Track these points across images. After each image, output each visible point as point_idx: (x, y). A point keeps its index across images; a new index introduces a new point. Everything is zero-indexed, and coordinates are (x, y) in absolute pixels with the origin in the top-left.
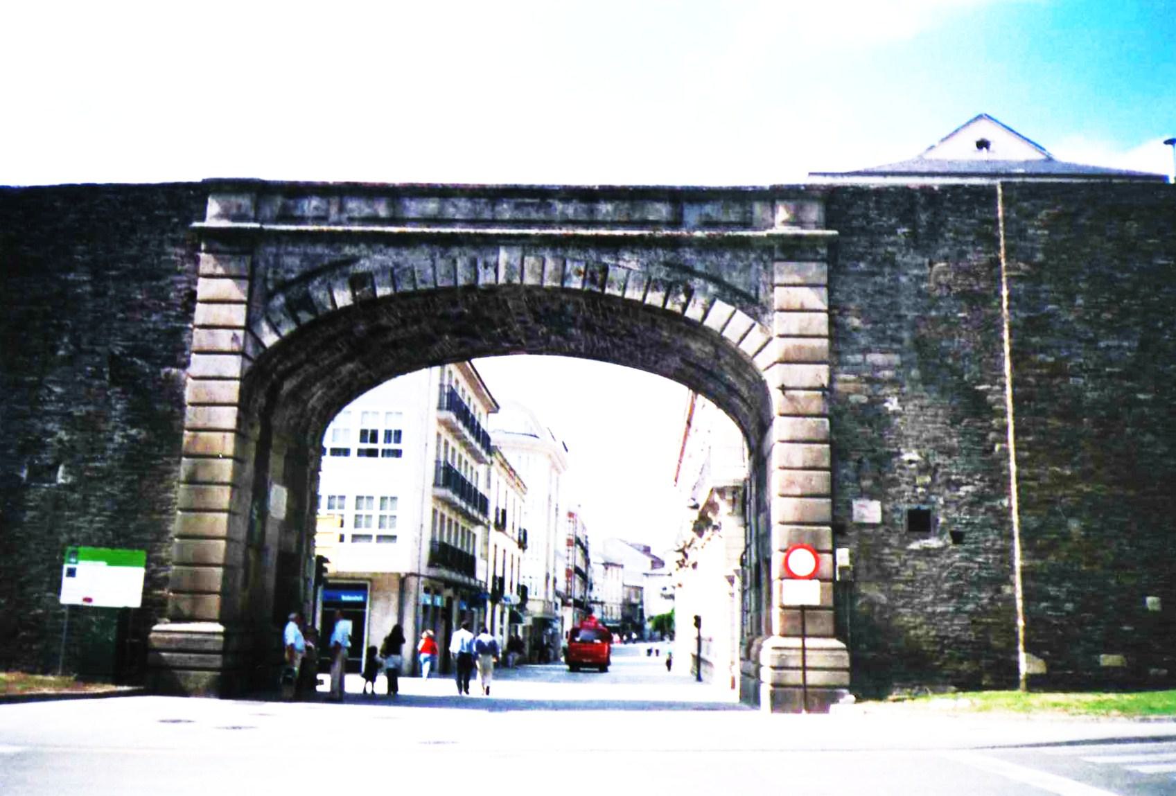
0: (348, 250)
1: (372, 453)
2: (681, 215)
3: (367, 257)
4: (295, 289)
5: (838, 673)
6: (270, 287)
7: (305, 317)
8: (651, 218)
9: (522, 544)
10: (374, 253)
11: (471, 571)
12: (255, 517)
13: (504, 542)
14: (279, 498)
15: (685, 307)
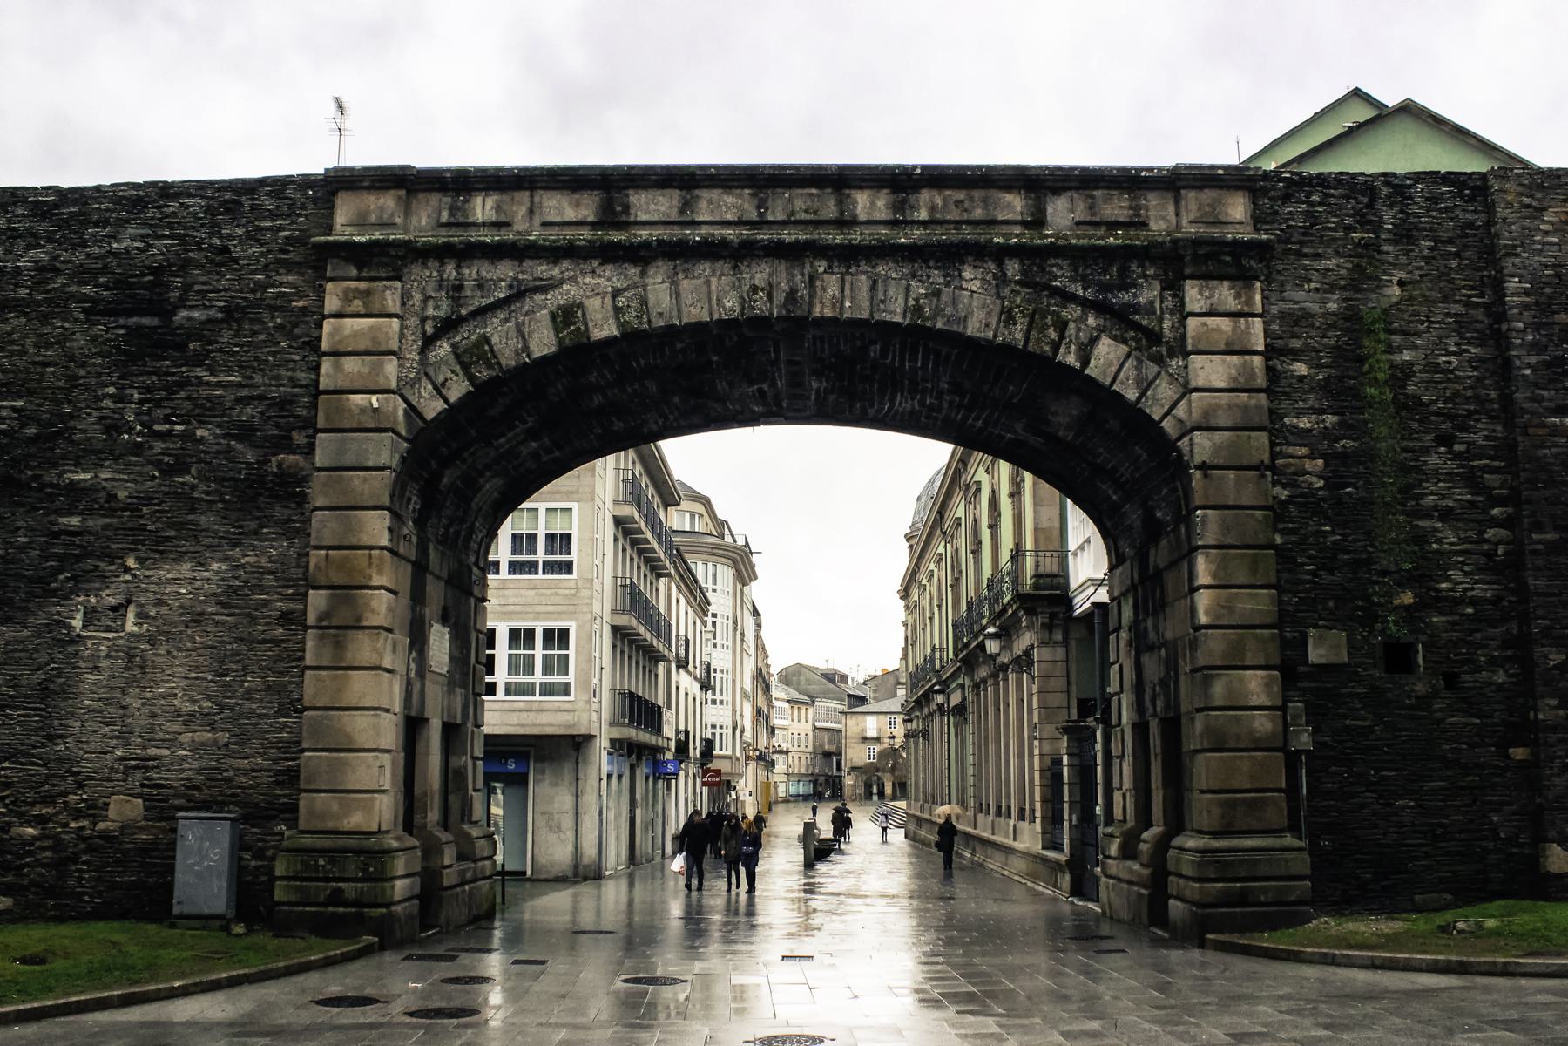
0: (542, 269)
1: (531, 567)
2: (1043, 211)
3: (573, 280)
4: (464, 331)
5: (312, 787)
6: (429, 329)
7: (483, 374)
8: (1000, 218)
9: (706, 685)
10: (584, 273)
11: (657, 729)
12: (412, 675)
13: (686, 682)
14: (440, 643)
15: (1056, 347)
